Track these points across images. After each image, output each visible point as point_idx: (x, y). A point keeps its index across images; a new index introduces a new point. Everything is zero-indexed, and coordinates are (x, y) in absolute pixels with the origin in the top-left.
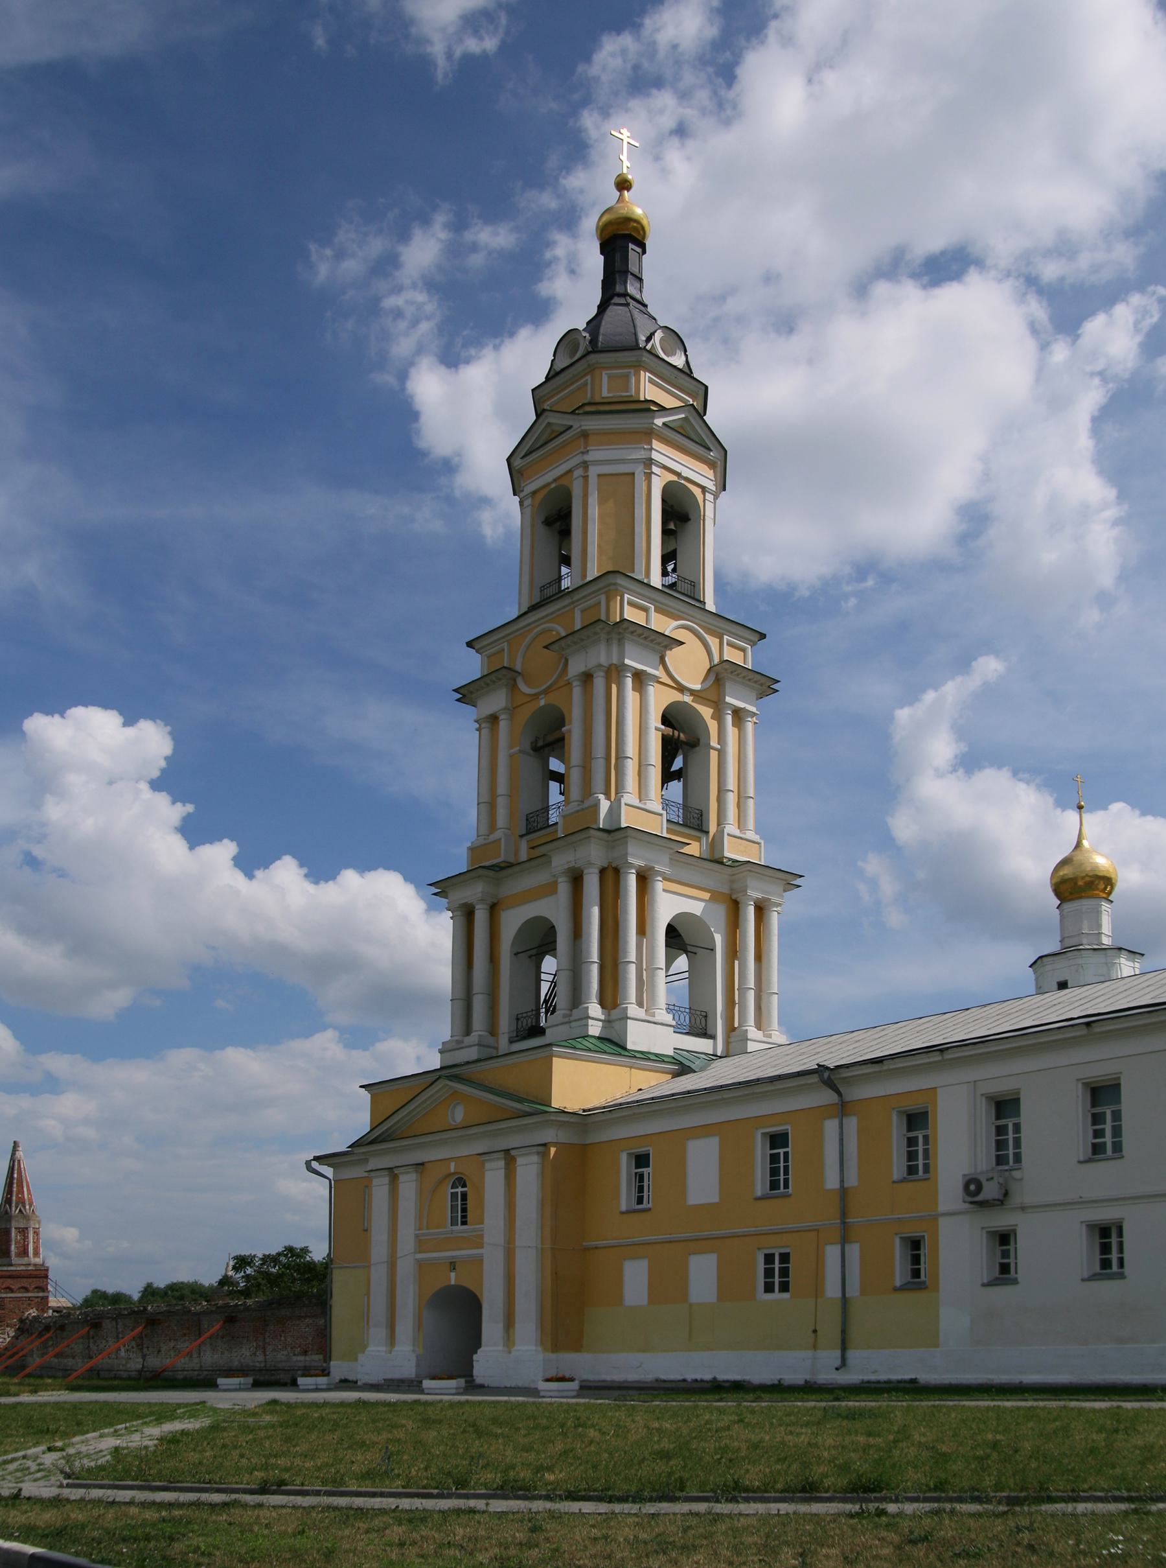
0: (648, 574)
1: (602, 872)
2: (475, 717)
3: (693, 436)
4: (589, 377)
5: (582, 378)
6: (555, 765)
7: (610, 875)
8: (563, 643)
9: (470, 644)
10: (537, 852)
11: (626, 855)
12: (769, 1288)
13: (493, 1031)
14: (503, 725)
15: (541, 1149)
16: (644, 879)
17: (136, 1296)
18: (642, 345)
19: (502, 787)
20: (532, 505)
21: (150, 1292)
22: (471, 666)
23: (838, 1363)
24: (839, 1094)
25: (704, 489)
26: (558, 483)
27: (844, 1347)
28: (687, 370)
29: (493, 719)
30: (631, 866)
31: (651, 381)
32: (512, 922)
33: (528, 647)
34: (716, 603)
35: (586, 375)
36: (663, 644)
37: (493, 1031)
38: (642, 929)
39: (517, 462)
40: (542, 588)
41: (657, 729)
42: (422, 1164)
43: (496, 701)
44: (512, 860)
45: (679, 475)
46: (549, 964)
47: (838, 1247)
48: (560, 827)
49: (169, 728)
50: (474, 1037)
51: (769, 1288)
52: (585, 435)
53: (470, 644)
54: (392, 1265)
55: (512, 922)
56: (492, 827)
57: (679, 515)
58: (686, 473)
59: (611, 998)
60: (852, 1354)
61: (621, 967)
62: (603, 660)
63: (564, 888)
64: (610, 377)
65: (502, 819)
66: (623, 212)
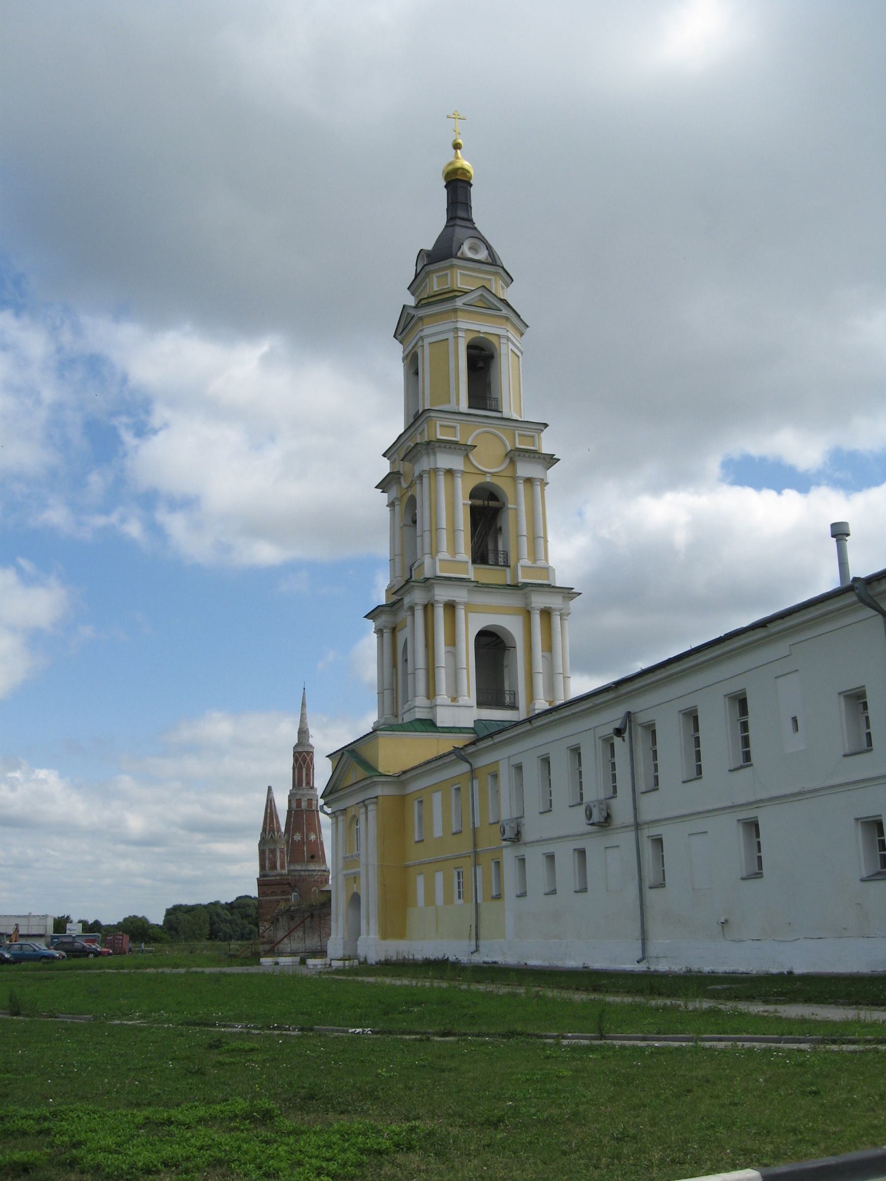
0: (458, 404)
3: (492, 307)
4: (449, 272)
7: (429, 607)
9: (384, 455)
11: (434, 596)
15: (375, 800)
16: (451, 607)
17: (254, 892)
18: (454, 252)
21: (125, 920)
23: (474, 948)
24: (471, 765)
26: (487, 336)
27: (477, 938)
30: (437, 602)
33: (487, 432)
36: (465, 450)
38: (452, 641)
42: (345, 810)
45: (479, 332)
47: (633, 834)
52: (421, 319)
53: (384, 455)
57: (481, 359)
58: (483, 329)
59: (431, 692)
60: (482, 942)
61: (436, 670)
62: (426, 468)
64: (438, 277)
66: (458, 165)
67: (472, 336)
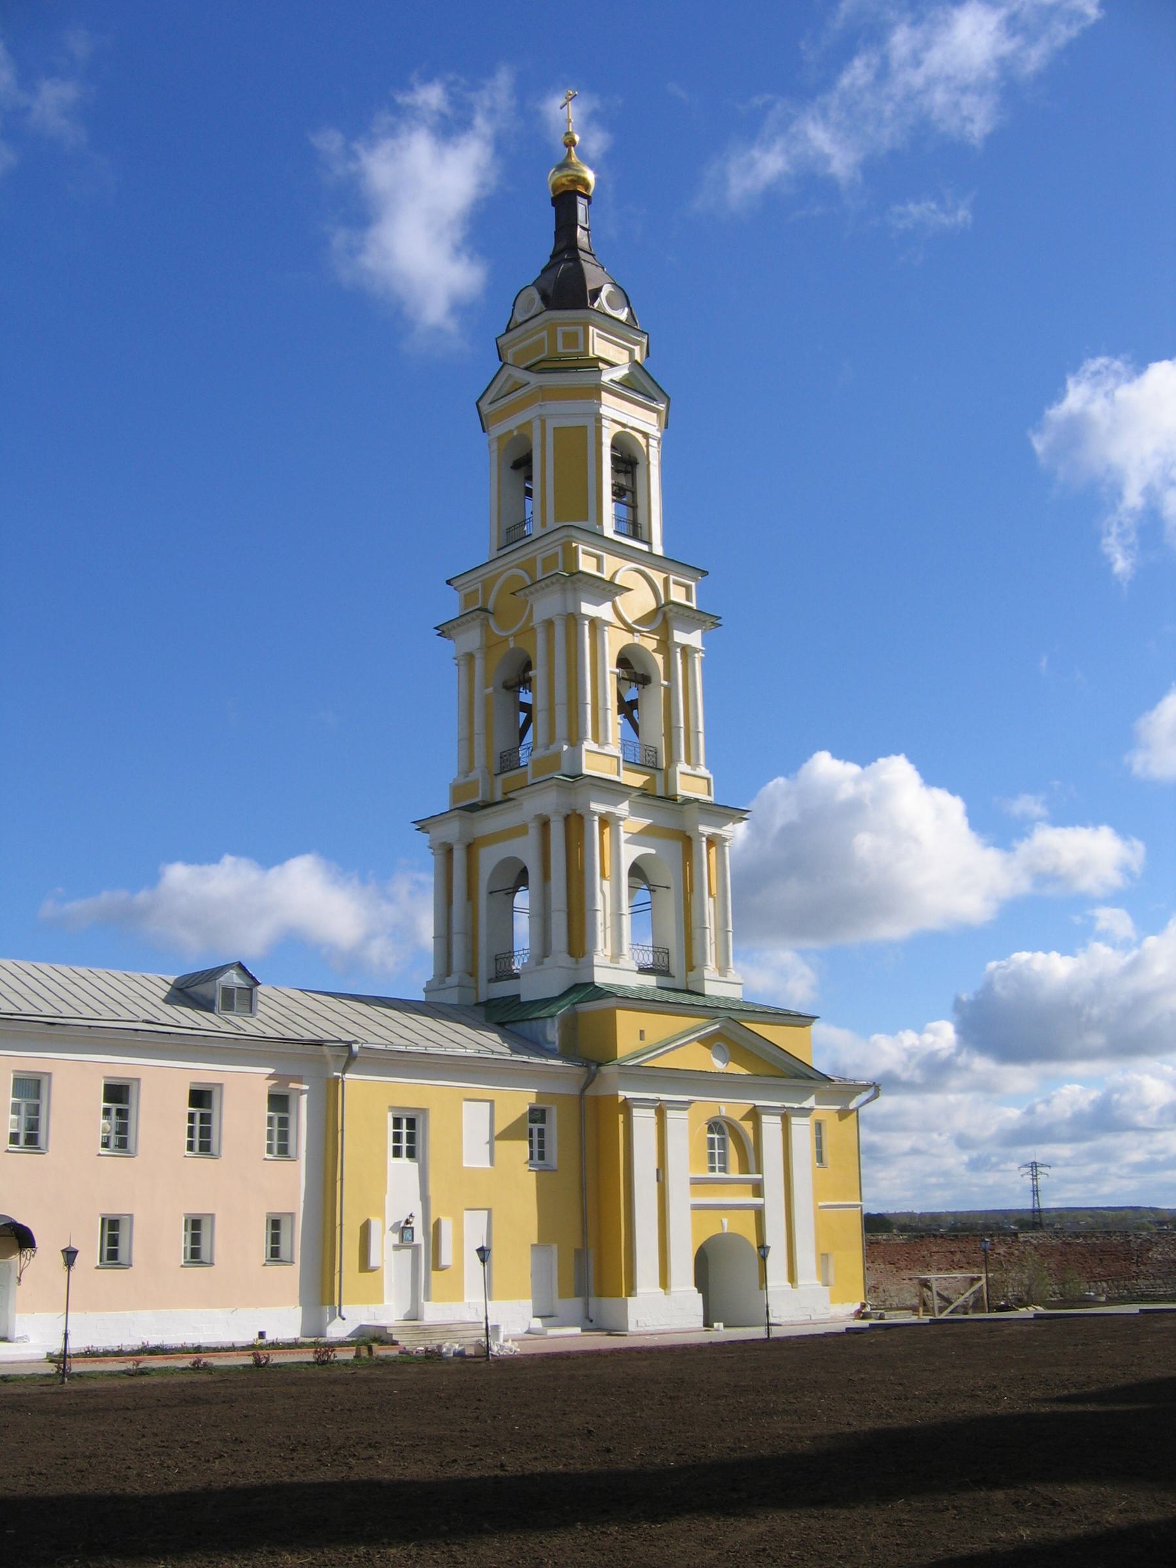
1: (567, 819)
2: (454, 655)
5: (537, 333)
6: (525, 697)
8: (527, 591)
9: (449, 582)
10: (506, 797)
12: (397, 1152)
13: (472, 973)
14: (479, 663)
19: (478, 726)
20: (499, 449)
22: (451, 606)
25: (646, 435)
28: (632, 323)
29: (470, 657)
31: (599, 336)
32: (489, 858)
34: (665, 543)
35: (541, 330)
37: (472, 973)
39: (484, 406)
40: (509, 531)
41: (612, 672)
43: (472, 639)
44: (488, 799)
45: (624, 426)
46: (522, 899)
48: (529, 769)
49: (579, 1525)
50: (453, 980)
51: (397, 1152)
54: (605, 928)
55: (489, 858)
56: (471, 768)
63: (533, 833)
65: (479, 760)
67: (619, 428)
